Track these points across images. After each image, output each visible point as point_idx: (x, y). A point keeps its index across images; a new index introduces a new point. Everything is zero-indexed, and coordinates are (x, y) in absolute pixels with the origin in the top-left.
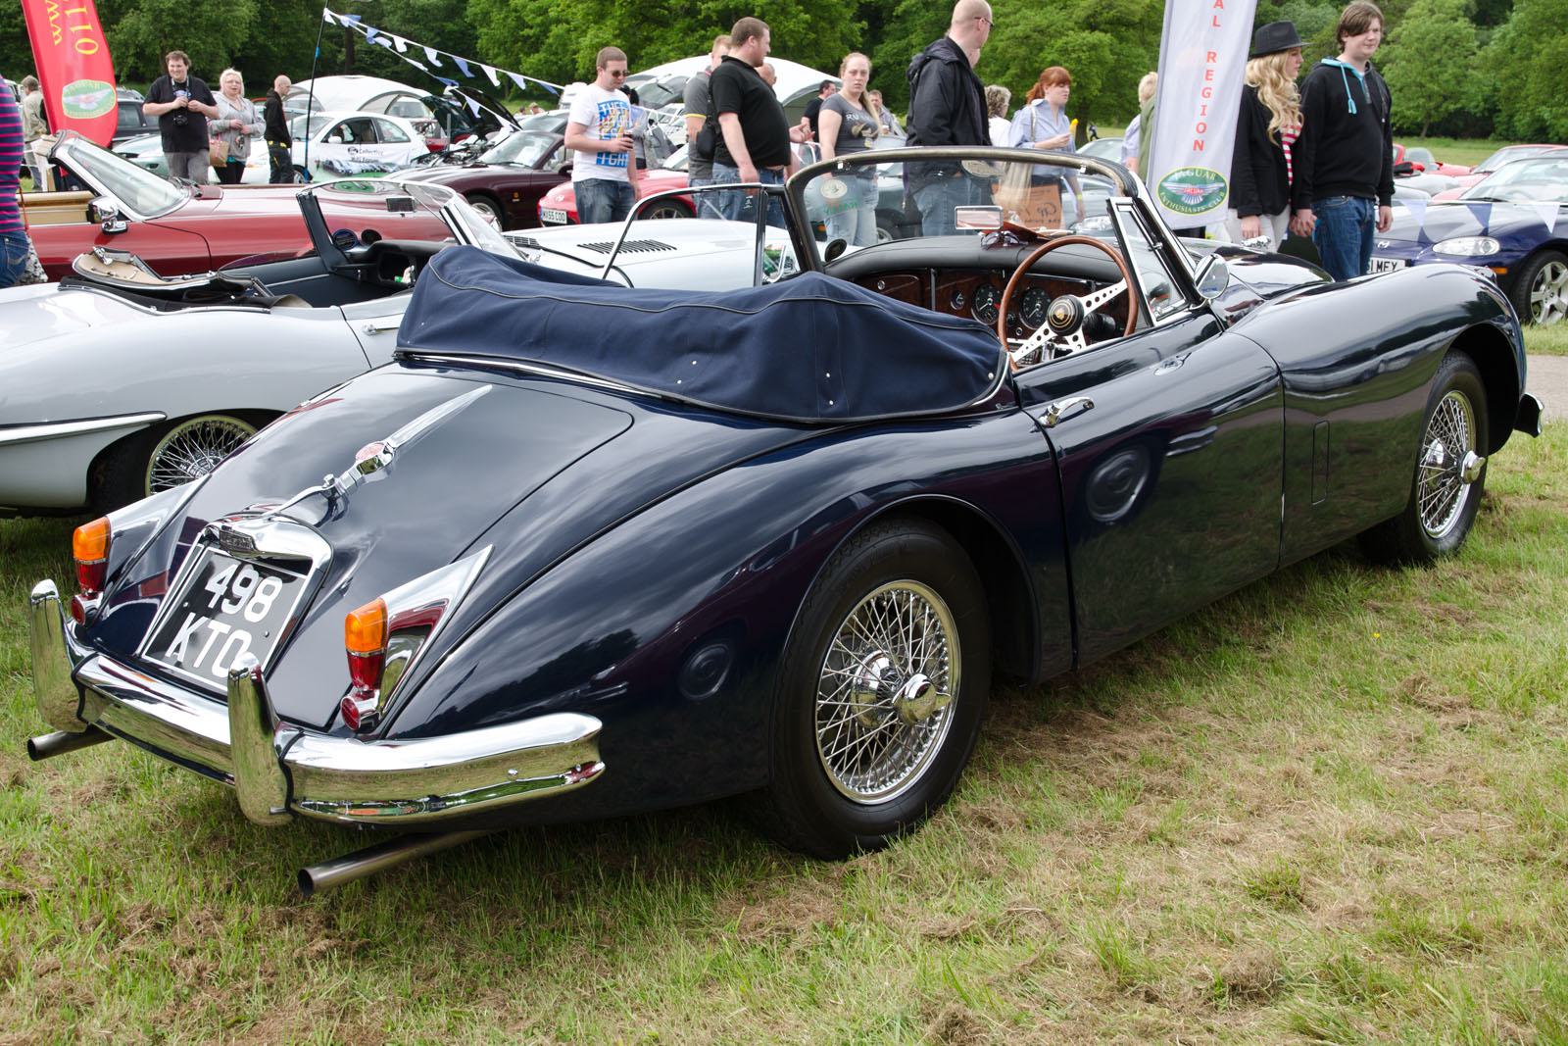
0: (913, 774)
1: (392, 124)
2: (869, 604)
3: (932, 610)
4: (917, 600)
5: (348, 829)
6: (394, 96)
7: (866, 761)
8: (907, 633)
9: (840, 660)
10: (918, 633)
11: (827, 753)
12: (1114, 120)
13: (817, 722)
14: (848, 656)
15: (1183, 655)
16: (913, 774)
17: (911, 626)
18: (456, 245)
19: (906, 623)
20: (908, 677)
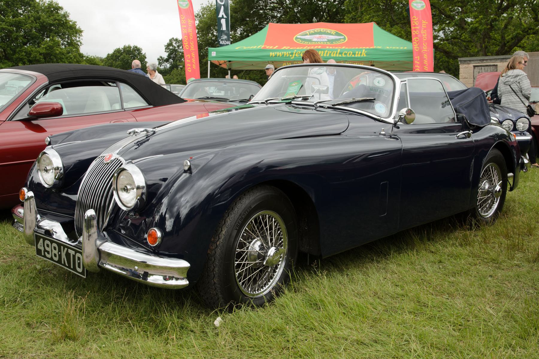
0: (268, 288)
1: (330, 34)
2: (251, 222)
3: (274, 220)
4: (269, 218)
5: (157, 289)
6: (66, 136)
7: (255, 281)
8: (267, 229)
9: (242, 245)
10: (271, 229)
11: (240, 281)
12: (62, 12)
13: (236, 270)
14: (245, 244)
15: (505, 50)
16: (268, 288)
17: (268, 227)
18: (31, 200)
19: (266, 225)
20: (269, 248)
